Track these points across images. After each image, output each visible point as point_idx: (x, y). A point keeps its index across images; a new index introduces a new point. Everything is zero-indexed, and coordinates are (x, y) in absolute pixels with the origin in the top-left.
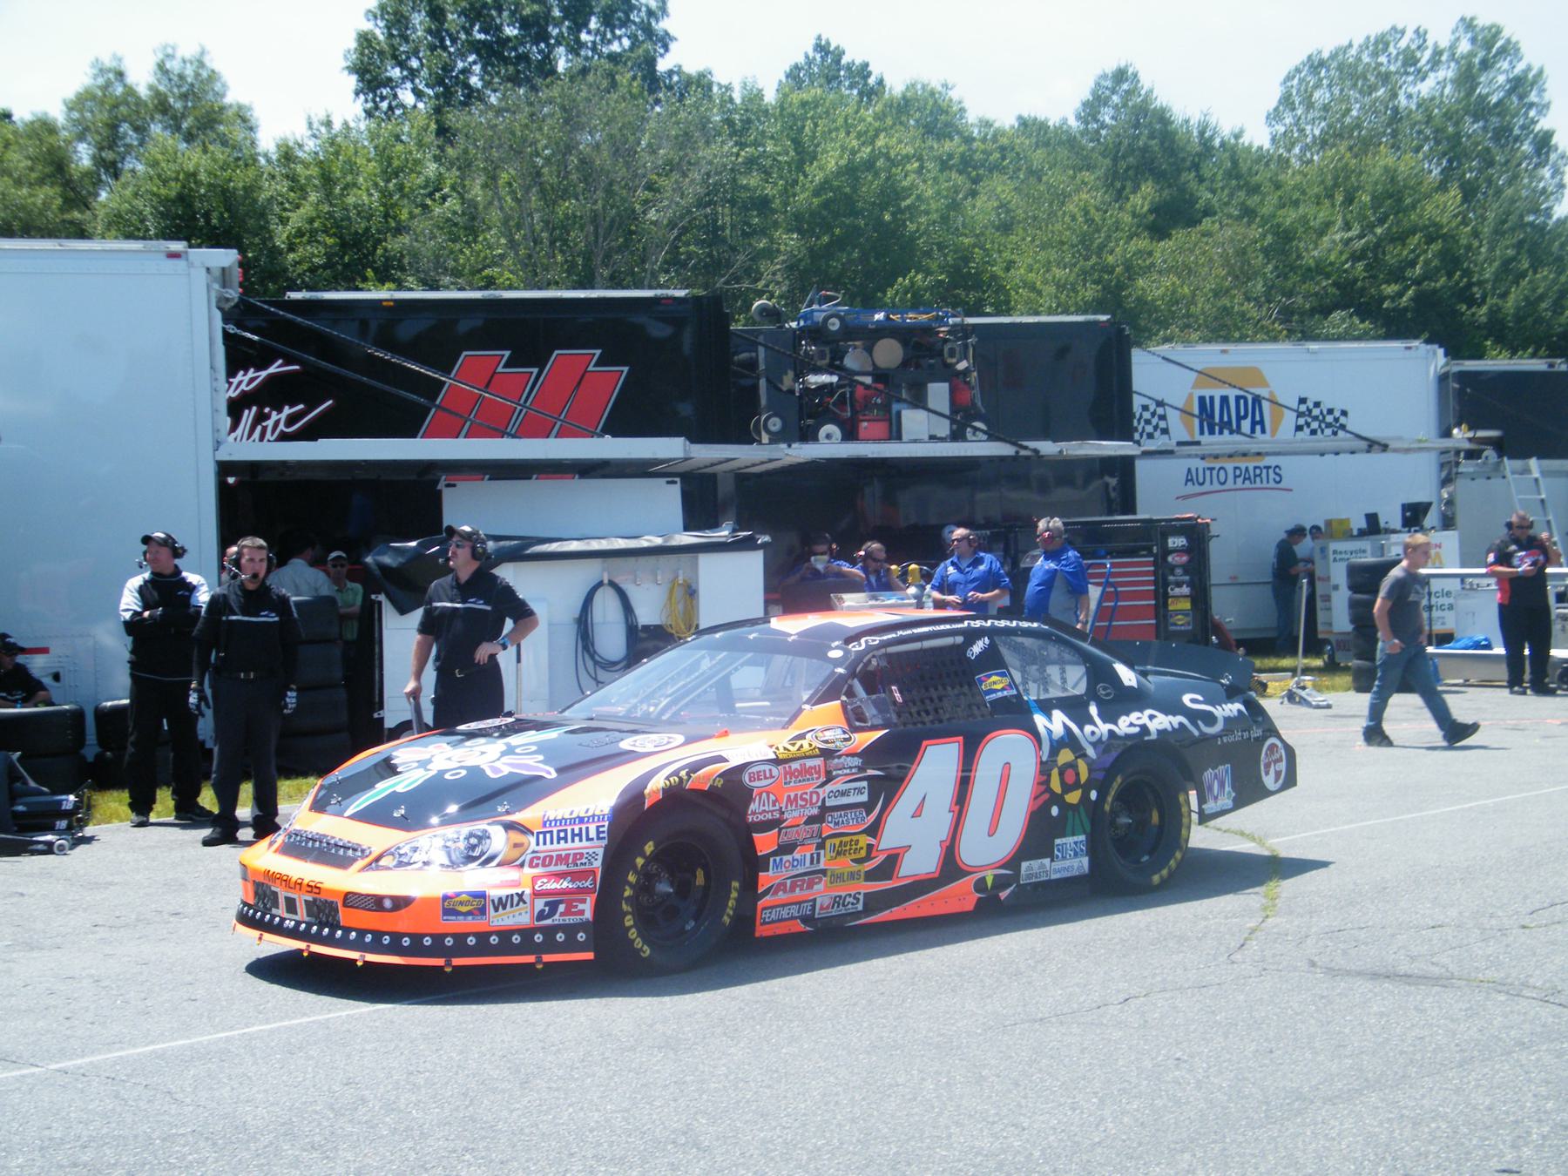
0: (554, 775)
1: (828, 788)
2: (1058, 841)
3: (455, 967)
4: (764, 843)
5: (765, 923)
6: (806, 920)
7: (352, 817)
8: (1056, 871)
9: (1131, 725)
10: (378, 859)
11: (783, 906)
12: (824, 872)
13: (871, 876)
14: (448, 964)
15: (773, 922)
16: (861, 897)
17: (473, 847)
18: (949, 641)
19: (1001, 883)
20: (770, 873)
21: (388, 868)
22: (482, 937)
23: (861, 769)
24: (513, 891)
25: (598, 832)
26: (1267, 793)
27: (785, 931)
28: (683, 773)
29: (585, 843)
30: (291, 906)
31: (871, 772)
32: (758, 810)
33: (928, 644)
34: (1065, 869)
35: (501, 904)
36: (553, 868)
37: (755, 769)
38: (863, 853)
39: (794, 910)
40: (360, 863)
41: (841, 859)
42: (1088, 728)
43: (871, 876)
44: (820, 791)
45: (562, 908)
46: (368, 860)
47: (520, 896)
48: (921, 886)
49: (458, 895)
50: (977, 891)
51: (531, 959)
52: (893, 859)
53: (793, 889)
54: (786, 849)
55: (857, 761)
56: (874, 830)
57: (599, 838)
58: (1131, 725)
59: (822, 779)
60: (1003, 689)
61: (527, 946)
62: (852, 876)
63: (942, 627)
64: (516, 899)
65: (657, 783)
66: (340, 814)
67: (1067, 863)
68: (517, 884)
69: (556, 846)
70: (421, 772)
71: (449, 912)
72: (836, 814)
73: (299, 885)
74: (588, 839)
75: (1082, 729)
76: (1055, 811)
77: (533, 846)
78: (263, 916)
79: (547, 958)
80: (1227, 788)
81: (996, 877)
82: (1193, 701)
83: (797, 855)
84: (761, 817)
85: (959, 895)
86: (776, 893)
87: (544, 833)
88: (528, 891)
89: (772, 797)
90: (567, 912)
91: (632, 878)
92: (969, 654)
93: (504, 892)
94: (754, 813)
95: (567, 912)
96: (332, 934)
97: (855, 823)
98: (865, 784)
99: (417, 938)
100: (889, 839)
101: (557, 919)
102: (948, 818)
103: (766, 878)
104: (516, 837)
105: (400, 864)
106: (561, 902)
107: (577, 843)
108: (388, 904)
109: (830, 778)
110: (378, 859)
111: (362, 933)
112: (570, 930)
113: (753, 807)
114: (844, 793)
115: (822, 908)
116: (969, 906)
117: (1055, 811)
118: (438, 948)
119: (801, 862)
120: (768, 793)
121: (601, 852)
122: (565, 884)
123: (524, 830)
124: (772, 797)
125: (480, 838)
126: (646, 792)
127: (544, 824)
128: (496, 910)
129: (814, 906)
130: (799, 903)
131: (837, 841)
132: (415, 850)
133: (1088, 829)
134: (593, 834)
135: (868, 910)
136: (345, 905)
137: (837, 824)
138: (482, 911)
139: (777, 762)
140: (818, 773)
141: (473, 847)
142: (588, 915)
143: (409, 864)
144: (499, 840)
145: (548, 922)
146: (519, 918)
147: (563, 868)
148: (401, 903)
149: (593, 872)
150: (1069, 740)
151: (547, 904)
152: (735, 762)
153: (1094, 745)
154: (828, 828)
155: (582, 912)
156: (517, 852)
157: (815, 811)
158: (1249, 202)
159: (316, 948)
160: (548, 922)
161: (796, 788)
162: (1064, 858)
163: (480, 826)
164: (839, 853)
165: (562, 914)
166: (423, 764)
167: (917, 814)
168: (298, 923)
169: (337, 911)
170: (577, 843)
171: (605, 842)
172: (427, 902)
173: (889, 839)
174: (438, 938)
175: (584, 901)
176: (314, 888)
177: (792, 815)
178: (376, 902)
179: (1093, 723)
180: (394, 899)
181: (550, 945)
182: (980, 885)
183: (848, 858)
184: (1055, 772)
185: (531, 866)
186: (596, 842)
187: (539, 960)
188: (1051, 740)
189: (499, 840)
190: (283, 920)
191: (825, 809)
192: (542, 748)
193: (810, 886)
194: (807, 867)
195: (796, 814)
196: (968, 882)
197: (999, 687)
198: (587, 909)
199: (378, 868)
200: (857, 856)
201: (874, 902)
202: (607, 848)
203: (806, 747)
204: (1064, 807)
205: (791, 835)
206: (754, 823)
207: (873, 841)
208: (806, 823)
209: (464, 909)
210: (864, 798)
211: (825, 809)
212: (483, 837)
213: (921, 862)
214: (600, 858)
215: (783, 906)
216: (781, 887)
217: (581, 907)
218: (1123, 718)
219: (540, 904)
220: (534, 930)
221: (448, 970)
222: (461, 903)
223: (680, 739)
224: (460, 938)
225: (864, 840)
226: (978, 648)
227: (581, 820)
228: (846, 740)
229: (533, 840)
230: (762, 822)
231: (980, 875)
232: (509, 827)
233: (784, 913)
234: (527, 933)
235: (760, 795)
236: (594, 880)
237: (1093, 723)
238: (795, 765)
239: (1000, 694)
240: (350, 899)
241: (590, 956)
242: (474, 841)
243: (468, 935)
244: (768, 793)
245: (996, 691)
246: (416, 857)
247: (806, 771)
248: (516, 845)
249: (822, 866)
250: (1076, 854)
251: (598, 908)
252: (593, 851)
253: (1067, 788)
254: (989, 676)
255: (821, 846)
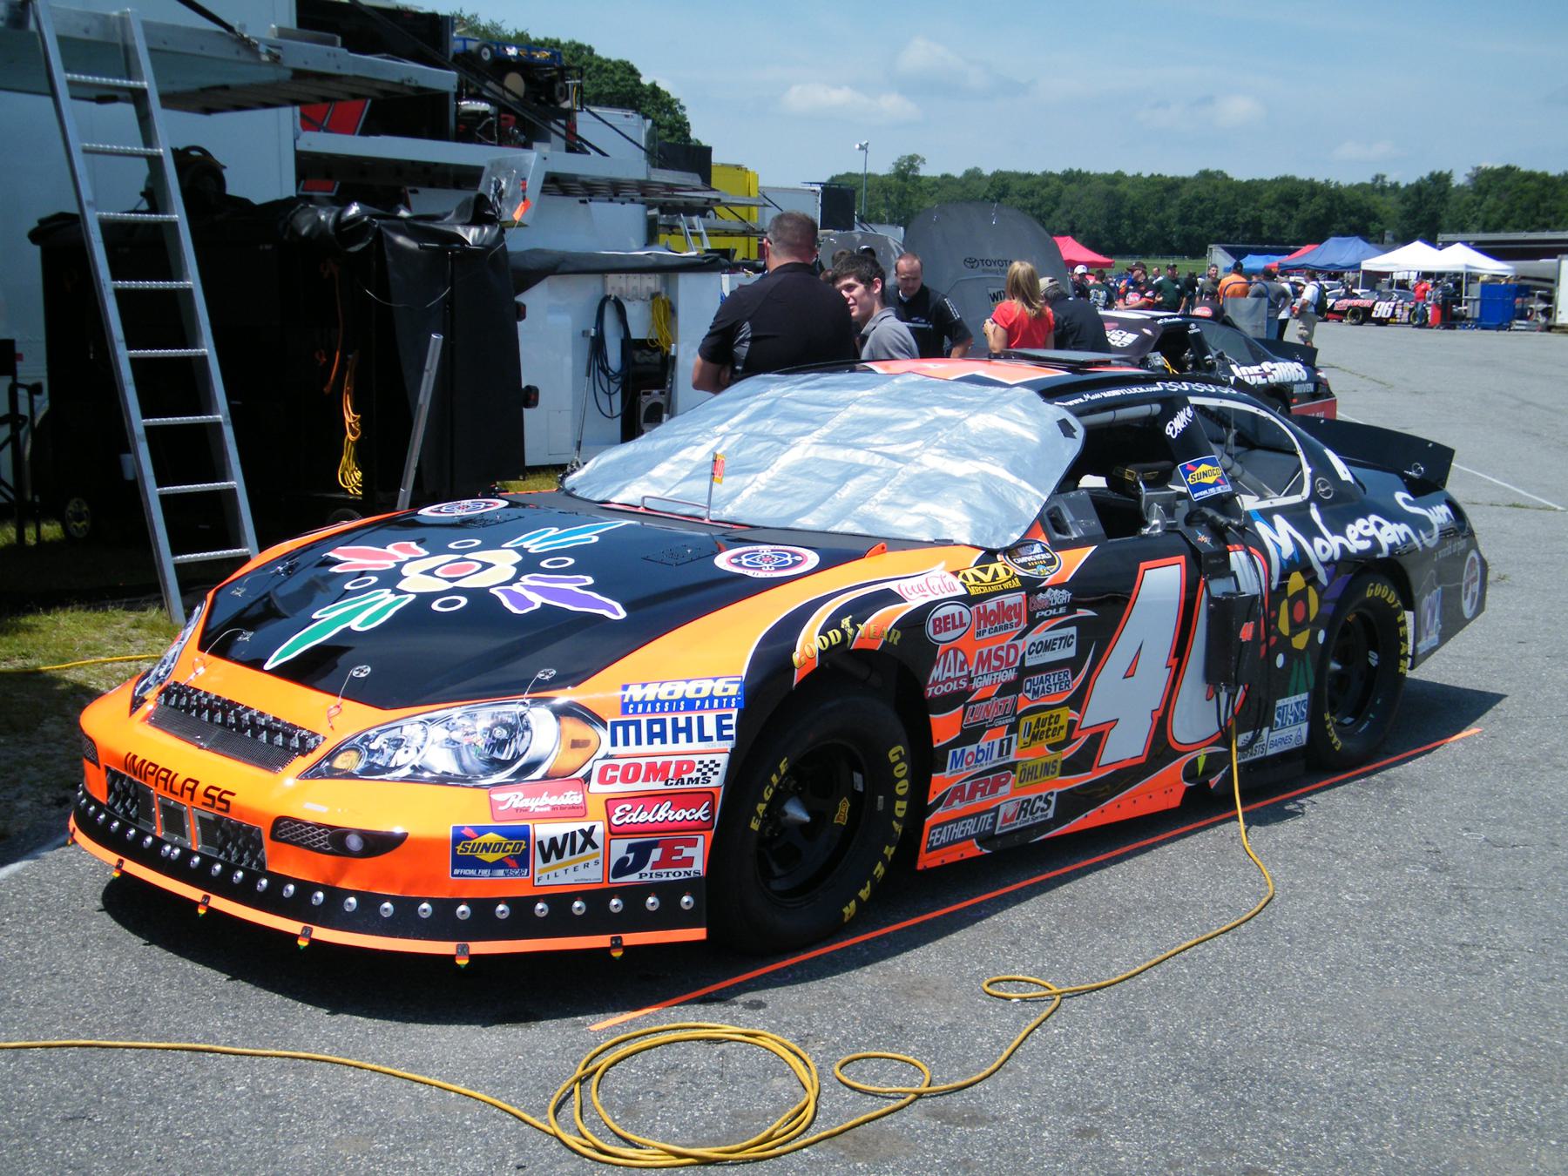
0: (623, 614)
1: (1031, 638)
2: (1280, 703)
3: (472, 957)
4: (944, 727)
5: (932, 849)
6: (985, 839)
7: (272, 672)
8: (1274, 744)
9: (1361, 537)
10: (332, 755)
11: (957, 820)
12: (1012, 766)
13: (1070, 767)
14: (463, 950)
15: (943, 845)
16: (1053, 799)
17: (501, 745)
18: (1143, 410)
19: (1216, 762)
20: (947, 774)
21: (349, 776)
22: (521, 906)
23: (1071, 607)
24: (574, 826)
25: (720, 727)
26: (1467, 622)
27: (956, 857)
28: (846, 622)
29: (696, 745)
30: (174, 819)
31: (1083, 612)
32: (942, 677)
33: (1123, 413)
34: (1283, 740)
35: (554, 849)
36: (640, 786)
37: (941, 613)
38: (1063, 734)
39: (970, 827)
40: (301, 763)
41: (1036, 745)
42: (1318, 542)
43: (1070, 767)
44: (1019, 643)
45: (656, 854)
46: (311, 759)
47: (587, 835)
48: (1127, 775)
49: (481, 831)
50: (1186, 779)
51: (602, 941)
52: (1097, 739)
53: (972, 796)
54: (970, 735)
55: (1065, 596)
56: (1078, 701)
57: (721, 737)
58: (1361, 537)
59: (1023, 625)
60: (1216, 484)
61: (597, 919)
62: (1046, 769)
63: (1135, 390)
64: (580, 840)
65: (809, 643)
66: (257, 664)
67: (1285, 733)
68: (579, 812)
69: (645, 748)
70: (386, 596)
71: (461, 862)
72: (1036, 678)
73: (190, 787)
74: (703, 738)
75: (1312, 544)
76: (1280, 661)
77: (606, 747)
78: (124, 828)
79: (630, 939)
80: (1437, 620)
81: (1209, 756)
82: (1406, 500)
83: (983, 744)
84: (944, 689)
85: (1164, 789)
86: (950, 803)
87: (626, 725)
88: (600, 828)
89: (961, 657)
90: (664, 862)
91: (879, 869)
92: (1169, 430)
93: (558, 829)
94: (936, 683)
95: (664, 862)
96: (251, 878)
97: (1057, 689)
98: (1073, 630)
99: (406, 906)
100: (1094, 714)
101: (647, 875)
102: (1164, 675)
103: (942, 781)
104: (576, 729)
105: (371, 771)
106: (655, 845)
107: (683, 745)
108: (354, 843)
109: (1033, 622)
110: (332, 755)
111: (306, 888)
112: (669, 892)
113: (936, 673)
114: (1048, 646)
115: (1005, 819)
116: (1175, 801)
117: (1280, 661)
118: (443, 923)
119: (987, 755)
120: (956, 650)
121: (723, 759)
122: (664, 813)
123: (590, 717)
124: (961, 657)
125: (512, 729)
126: (796, 657)
127: (625, 708)
128: (546, 859)
129: (995, 818)
130: (978, 815)
131: (1033, 719)
132: (398, 744)
133: (1312, 686)
134: (711, 729)
135: (1058, 820)
136: (274, 836)
137: (1035, 693)
138: (522, 860)
139: (968, 600)
140: (1018, 615)
141: (501, 745)
142: (699, 866)
143: (387, 769)
144: (545, 735)
145: (633, 878)
146: (585, 872)
147: (658, 785)
148: (379, 844)
149: (710, 794)
150: (1300, 563)
151: (631, 848)
152: (915, 602)
153: (1324, 564)
154: (1026, 700)
155: (689, 861)
156: (576, 757)
157: (1011, 675)
158: (309, 216)
159: (220, 903)
160: (633, 878)
161: (989, 641)
162: (1284, 725)
163: (511, 709)
164: (1034, 737)
165: (656, 865)
166: (391, 579)
167: (1129, 674)
168: (187, 854)
169: (260, 845)
170: (683, 745)
171: (728, 745)
172: (427, 846)
173: (1094, 714)
174: (444, 907)
175: (693, 843)
176: (218, 798)
177: (985, 683)
178: (336, 840)
179: (1322, 536)
180: (365, 835)
181: (636, 918)
182: (1190, 771)
183: (1043, 744)
184: (1284, 604)
185: (602, 780)
186: (716, 744)
187: (617, 944)
188: (1281, 559)
189: (545, 735)
190: (159, 843)
191: (1024, 672)
192: (585, 560)
193: (994, 790)
194: (995, 760)
195: (987, 681)
196: (1177, 767)
197: (1210, 480)
198: (697, 856)
199: (332, 774)
200: (1052, 740)
201: (1071, 803)
202: (734, 754)
203: (1002, 575)
204: (1291, 654)
205: (979, 714)
206: (934, 697)
207: (1075, 716)
208: (999, 694)
209: (490, 857)
210: (1070, 652)
211: (1024, 672)
212: (517, 728)
213: (1125, 746)
214: (722, 770)
215: (957, 820)
216: (958, 793)
217: (687, 852)
218: (1350, 527)
219: (620, 848)
220: (606, 894)
221: (462, 962)
222: (486, 847)
223: (813, 559)
224: (483, 907)
225: (1067, 714)
226: (1178, 424)
227: (690, 704)
228: (1051, 562)
229: (606, 736)
230: (944, 695)
231: (1189, 757)
232: (561, 713)
233: (958, 831)
234: (595, 898)
235: (946, 653)
236: (712, 808)
237: (1322, 536)
238: (991, 605)
239: (1213, 492)
240: (287, 829)
241: (698, 934)
242: (501, 733)
243: (498, 901)
244: (956, 650)
245: (1206, 486)
246: (400, 757)
247: (1004, 612)
248: (575, 744)
249: (1012, 758)
250: (1296, 720)
251: (715, 857)
252: (709, 755)
253: (1296, 627)
254: (1198, 465)
255: (1014, 728)
